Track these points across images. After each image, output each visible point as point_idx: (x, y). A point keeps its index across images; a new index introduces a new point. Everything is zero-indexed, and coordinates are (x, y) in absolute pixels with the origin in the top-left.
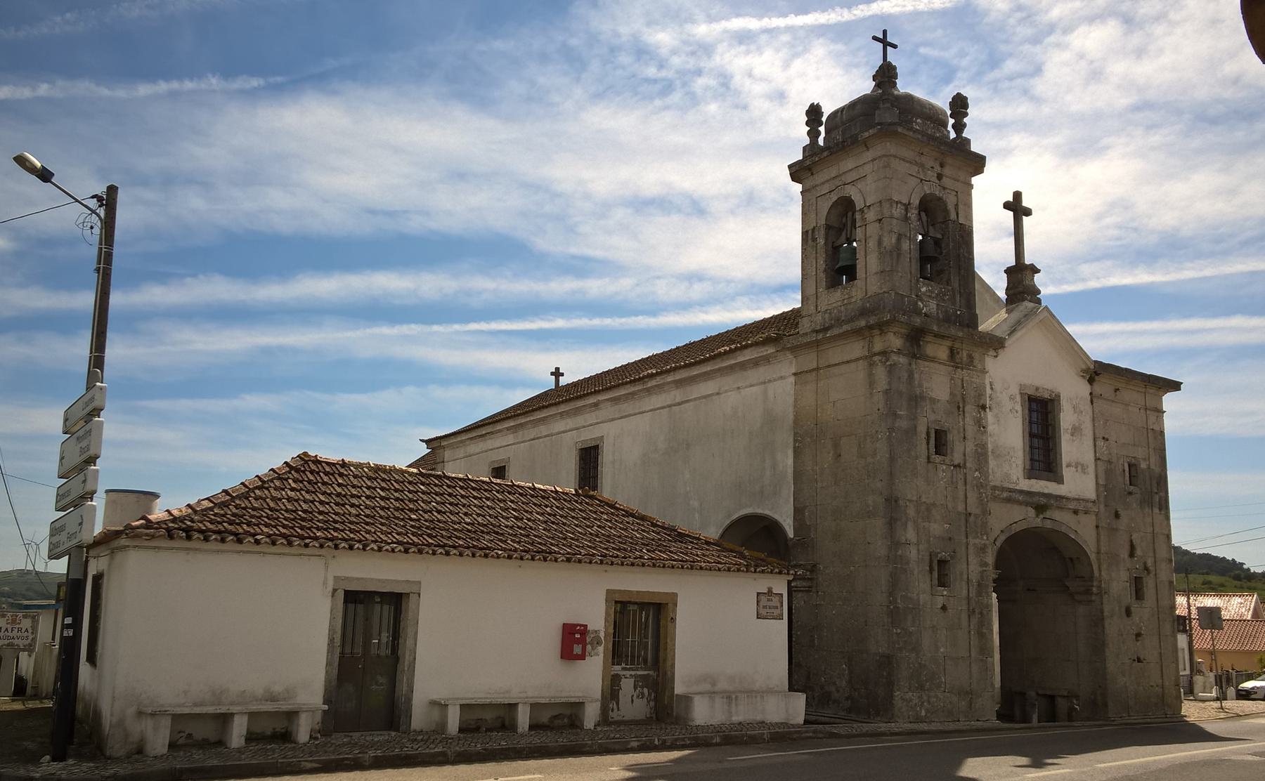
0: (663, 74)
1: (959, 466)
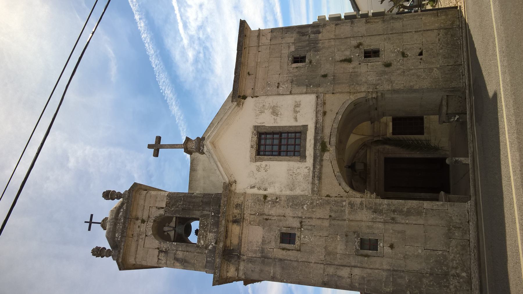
0: (202, 51)
1: (301, 222)
